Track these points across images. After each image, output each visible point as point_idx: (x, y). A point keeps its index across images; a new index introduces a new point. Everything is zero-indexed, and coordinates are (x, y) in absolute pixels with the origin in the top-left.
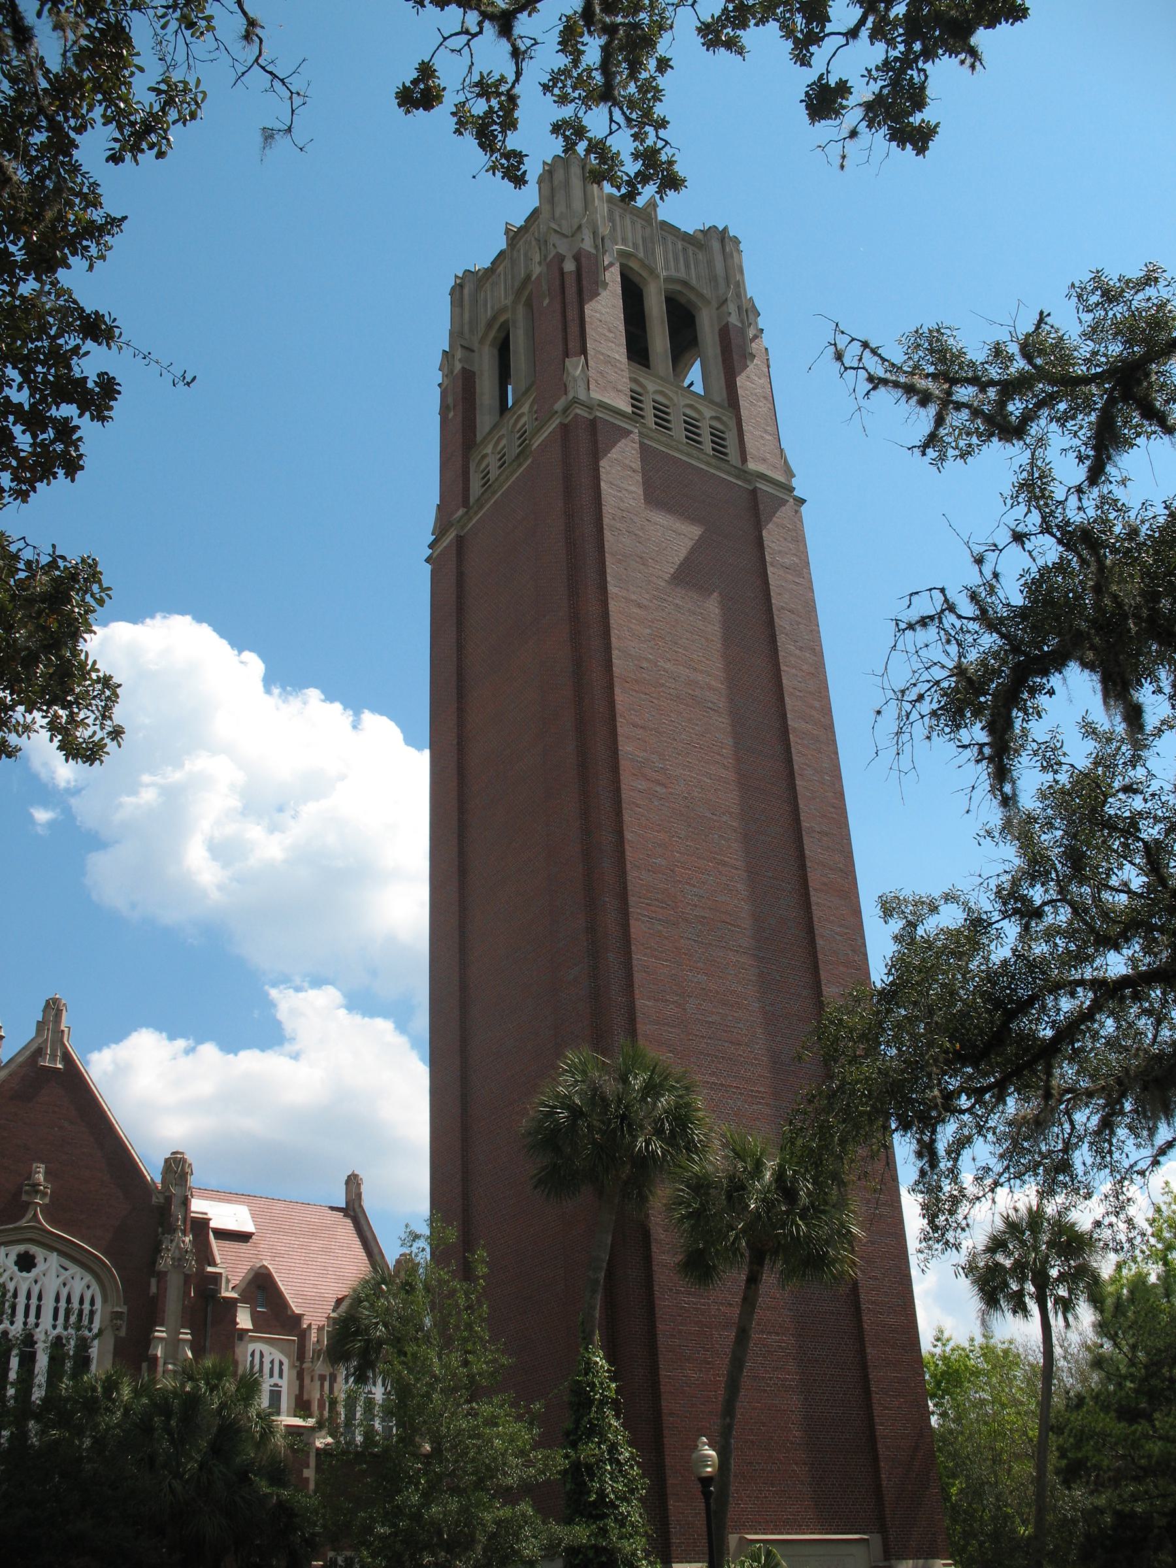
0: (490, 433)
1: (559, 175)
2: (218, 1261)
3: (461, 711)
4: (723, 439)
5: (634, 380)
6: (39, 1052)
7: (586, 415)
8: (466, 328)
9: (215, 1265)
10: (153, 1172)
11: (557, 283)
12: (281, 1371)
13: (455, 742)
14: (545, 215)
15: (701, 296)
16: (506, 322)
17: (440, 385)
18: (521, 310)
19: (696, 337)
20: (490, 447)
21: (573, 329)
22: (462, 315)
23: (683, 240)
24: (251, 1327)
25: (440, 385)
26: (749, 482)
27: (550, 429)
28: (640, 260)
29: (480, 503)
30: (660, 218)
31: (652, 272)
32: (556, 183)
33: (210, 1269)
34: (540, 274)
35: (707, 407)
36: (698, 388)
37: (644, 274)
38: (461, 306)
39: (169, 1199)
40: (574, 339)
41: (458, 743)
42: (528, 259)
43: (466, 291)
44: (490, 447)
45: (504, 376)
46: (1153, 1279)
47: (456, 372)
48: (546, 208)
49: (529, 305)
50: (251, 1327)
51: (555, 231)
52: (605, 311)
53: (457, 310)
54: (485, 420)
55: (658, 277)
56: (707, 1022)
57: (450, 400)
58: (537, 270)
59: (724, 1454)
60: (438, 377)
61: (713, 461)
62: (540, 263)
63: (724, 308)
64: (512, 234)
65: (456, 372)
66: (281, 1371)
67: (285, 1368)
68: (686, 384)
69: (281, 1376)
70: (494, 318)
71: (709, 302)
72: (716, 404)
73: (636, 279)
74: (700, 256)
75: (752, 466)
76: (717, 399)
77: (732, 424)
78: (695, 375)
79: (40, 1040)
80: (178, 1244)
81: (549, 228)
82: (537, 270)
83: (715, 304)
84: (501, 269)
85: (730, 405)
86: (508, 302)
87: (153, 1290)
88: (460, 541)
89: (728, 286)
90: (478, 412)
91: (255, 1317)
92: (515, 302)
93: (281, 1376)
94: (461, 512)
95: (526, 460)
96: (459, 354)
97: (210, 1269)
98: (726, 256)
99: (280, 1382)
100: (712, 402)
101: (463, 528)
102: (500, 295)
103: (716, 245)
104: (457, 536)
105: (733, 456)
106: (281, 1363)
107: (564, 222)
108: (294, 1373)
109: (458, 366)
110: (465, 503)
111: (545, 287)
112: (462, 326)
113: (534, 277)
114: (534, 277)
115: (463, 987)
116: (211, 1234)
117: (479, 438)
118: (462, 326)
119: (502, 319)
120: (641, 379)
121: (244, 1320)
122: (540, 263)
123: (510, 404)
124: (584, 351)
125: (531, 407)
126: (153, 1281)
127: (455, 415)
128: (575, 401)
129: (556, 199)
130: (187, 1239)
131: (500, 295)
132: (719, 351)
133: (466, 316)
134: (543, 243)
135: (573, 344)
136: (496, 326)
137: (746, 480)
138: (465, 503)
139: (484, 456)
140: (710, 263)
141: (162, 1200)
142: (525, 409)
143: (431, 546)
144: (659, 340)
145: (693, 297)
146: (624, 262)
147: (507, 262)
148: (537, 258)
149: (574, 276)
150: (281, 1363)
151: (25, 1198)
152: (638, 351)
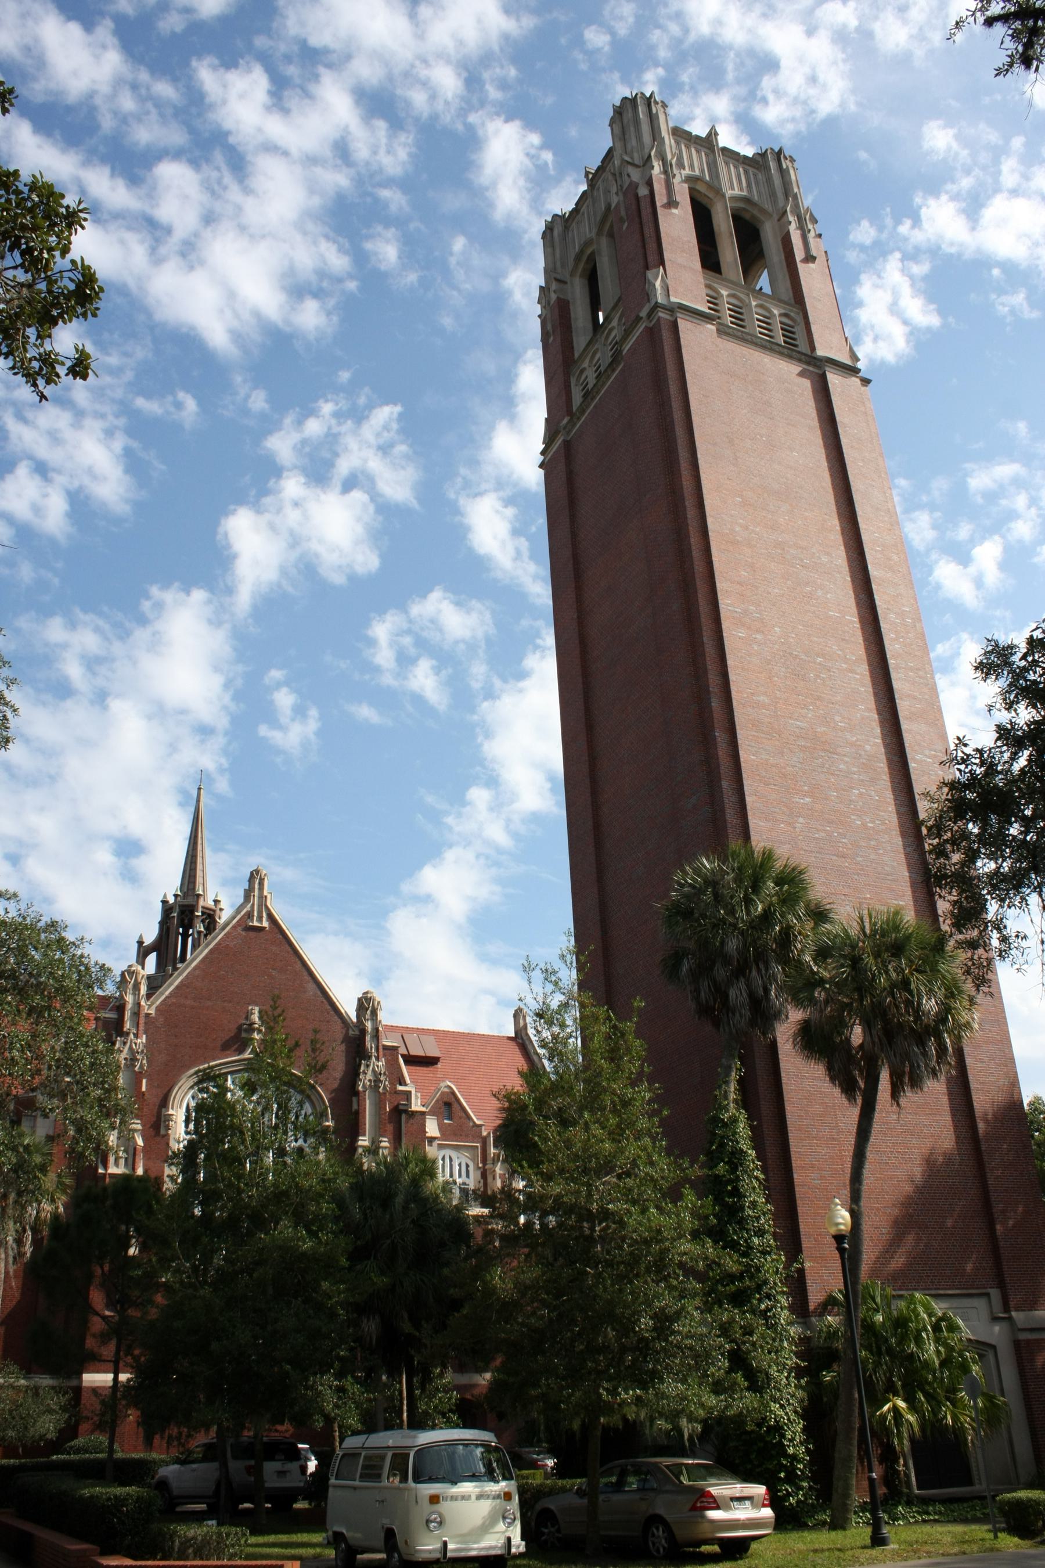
0: (585, 350)
1: (628, 115)
2: (408, 1081)
3: (579, 588)
4: (793, 333)
5: (708, 286)
6: (249, 915)
7: (668, 317)
8: (558, 264)
9: (406, 1085)
10: (349, 1008)
11: (634, 207)
12: (468, 1172)
13: (575, 616)
14: (616, 154)
15: (763, 211)
16: (593, 254)
17: (539, 316)
18: (604, 241)
19: (762, 249)
20: (587, 361)
21: (651, 245)
22: (554, 254)
23: (743, 163)
24: (438, 1135)
25: (539, 316)
26: (819, 367)
27: (637, 334)
28: (706, 183)
29: (582, 410)
30: (721, 145)
31: (719, 192)
32: (625, 121)
33: (400, 1088)
34: (618, 203)
35: (775, 305)
36: (767, 290)
37: (711, 195)
38: (553, 246)
39: (363, 1032)
40: (650, 252)
41: (578, 617)
42: (607, 192)
43: (556, 232)
44: (587, 361)
45: (595, 305)
46: (168, 1186)
47: (552, 302)
48: (619, 145)
49: (611, 235)
50: (438, 1135)
51: (628, 163)
52: (677, 228)
53: (549, 250)
54: (580, 341)
55: (724, 196)
56: (814, 838)
57: (549, 327)
58: (615, 200)
59: (855, 1215)
60: (538, 309)
61: (786, 351)
62: (617, 194)
63: (784, 219)
64: (590, 176)
65: (552, 302)
66: (468, 1172)
67: (471, 1169)
68: (758, 288)
69: (468, 1176)
70: (582, 252)
71: (770, 215)
72: (785, 303)
73: (704, 201)
74: (760, 176)
75: (820, 352)
76: (784, 297)
77: (800, 319)
78: (764, 282)
79: (248, 908)
80: (131, 1046)
81: (623, 160)
82: (615, 200)
83: (776, 217)
84: (584, 209)
85: (796, 303)
86: (593, 234)
87: (355, 1107)
88: (567, 445)
89: (787, 199)
90: (574, 334)
91: (441, 1127)
92: (600, 233)
93: (468, 1176)
94: (565, 421)
95: (617, 366)
96: (554, 286)
97: (400, 1088)
98: (783, 173)
99: (467, 1181)
100: (780, 301)
101: (568, 433)
102: (585, 230)
103: (773, 165)
104: (564, 441)
105: (803, 347)
106: (467, 1166)
107: (636, 155)
108: (479, 1173)
109: (554, 297)
110: (570, 412)
111: (623, 213)
112: (555, 263)
113: (613, 206)
114: (613, 206)
115: (597, 827)
116: (401, 1060)
117: (576, 355)
118: (555, 263)
119: (589, 251)
120: (716, 285)
121: (432, 1128)
122: (617, 194)
123: (601, 320)
124: (662, 263)
125: (620, 320)
126: (354, 1099)
127: (554, 340)
128: (657, 305)
129: (627, 136)
130: (380, 1063)
131: (585, 230)
132: (783, 257)
133: (558, 255)
134: (618, 175)
135: (652, 258)
136: (585, 258)
137: (815, 366)
138: (570, 412)
139: (582, 371)
140: (769, 180)
141: (357, 1033)
142: (614, 323)
143: (543, 453)
144: (729, 252)
145: (755, 212)
146: (692, 186)
147: (589, 201)
148: (614, 189)
149: (648, 199)
150: (467, 1166)
151: (244, 1035)
152: (710, 261)
